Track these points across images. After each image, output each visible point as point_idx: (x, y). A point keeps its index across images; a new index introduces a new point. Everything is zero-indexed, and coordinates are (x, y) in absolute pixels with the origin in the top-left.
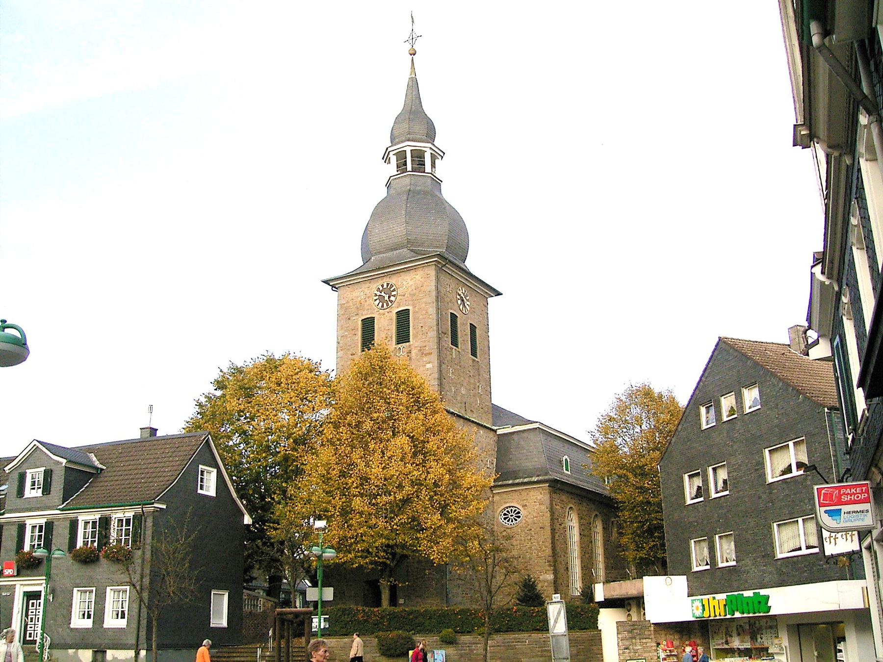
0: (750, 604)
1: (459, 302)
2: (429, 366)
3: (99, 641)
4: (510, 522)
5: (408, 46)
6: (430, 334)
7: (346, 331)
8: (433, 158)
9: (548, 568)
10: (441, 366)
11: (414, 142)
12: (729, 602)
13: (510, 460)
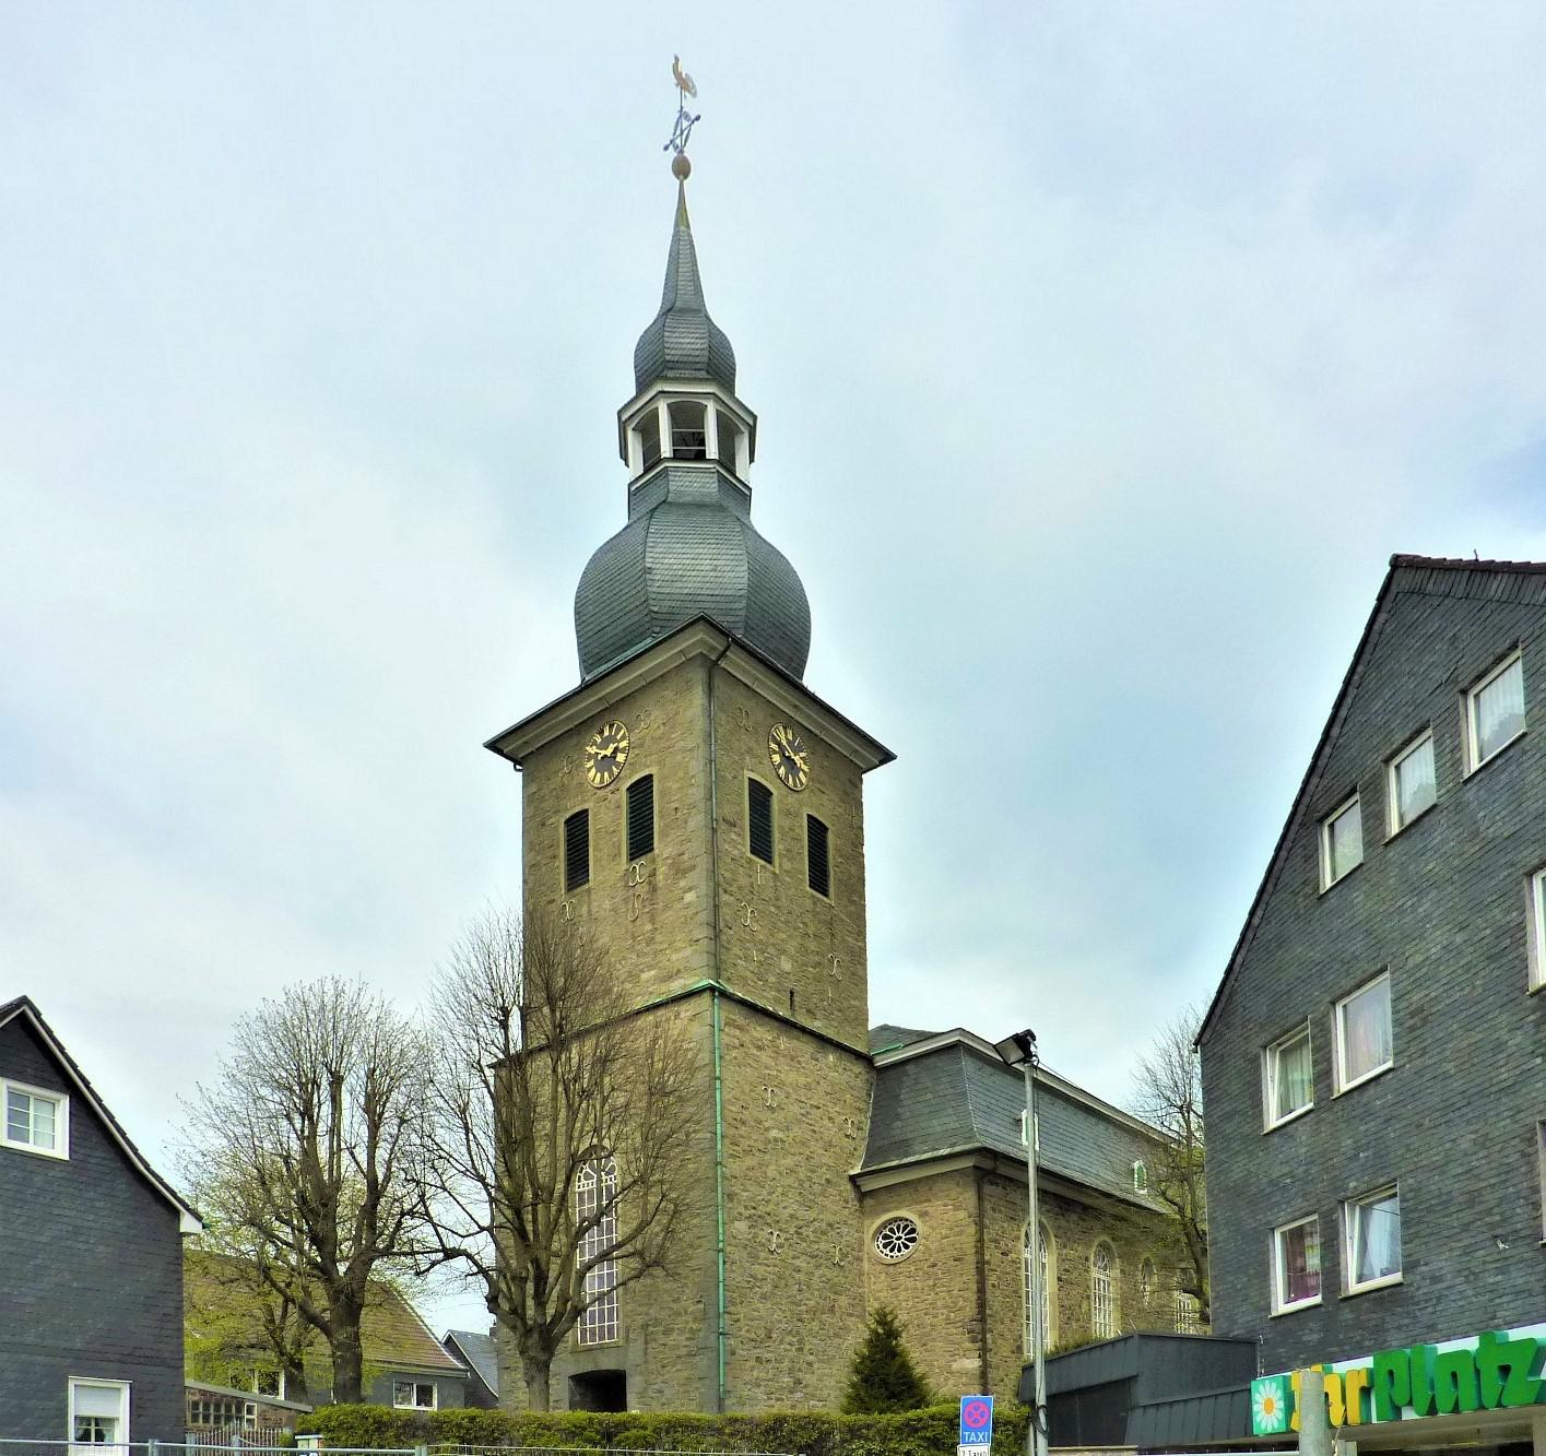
0: (1467, 1381)
1: (777, 758)
2: (690, 897)
3: (94, 1431)
4: (895, 1253)
5: (672, 154)
6: (692, 824)
7: (538, 853)
8: (727, 433)
9: (968, 1345)
10: (716, 894)
11: (687, 407)
12: (1382, 1379)
13: (898, 1117)
